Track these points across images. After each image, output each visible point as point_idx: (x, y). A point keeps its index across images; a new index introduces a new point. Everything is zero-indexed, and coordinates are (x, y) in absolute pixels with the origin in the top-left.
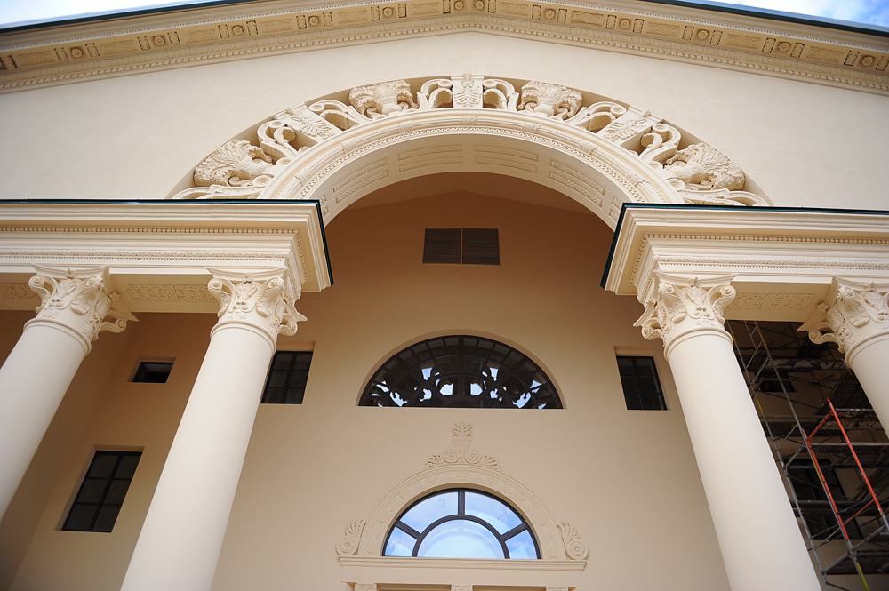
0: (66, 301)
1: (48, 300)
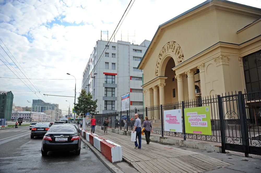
0: (189, 74)
1: (177, 78)
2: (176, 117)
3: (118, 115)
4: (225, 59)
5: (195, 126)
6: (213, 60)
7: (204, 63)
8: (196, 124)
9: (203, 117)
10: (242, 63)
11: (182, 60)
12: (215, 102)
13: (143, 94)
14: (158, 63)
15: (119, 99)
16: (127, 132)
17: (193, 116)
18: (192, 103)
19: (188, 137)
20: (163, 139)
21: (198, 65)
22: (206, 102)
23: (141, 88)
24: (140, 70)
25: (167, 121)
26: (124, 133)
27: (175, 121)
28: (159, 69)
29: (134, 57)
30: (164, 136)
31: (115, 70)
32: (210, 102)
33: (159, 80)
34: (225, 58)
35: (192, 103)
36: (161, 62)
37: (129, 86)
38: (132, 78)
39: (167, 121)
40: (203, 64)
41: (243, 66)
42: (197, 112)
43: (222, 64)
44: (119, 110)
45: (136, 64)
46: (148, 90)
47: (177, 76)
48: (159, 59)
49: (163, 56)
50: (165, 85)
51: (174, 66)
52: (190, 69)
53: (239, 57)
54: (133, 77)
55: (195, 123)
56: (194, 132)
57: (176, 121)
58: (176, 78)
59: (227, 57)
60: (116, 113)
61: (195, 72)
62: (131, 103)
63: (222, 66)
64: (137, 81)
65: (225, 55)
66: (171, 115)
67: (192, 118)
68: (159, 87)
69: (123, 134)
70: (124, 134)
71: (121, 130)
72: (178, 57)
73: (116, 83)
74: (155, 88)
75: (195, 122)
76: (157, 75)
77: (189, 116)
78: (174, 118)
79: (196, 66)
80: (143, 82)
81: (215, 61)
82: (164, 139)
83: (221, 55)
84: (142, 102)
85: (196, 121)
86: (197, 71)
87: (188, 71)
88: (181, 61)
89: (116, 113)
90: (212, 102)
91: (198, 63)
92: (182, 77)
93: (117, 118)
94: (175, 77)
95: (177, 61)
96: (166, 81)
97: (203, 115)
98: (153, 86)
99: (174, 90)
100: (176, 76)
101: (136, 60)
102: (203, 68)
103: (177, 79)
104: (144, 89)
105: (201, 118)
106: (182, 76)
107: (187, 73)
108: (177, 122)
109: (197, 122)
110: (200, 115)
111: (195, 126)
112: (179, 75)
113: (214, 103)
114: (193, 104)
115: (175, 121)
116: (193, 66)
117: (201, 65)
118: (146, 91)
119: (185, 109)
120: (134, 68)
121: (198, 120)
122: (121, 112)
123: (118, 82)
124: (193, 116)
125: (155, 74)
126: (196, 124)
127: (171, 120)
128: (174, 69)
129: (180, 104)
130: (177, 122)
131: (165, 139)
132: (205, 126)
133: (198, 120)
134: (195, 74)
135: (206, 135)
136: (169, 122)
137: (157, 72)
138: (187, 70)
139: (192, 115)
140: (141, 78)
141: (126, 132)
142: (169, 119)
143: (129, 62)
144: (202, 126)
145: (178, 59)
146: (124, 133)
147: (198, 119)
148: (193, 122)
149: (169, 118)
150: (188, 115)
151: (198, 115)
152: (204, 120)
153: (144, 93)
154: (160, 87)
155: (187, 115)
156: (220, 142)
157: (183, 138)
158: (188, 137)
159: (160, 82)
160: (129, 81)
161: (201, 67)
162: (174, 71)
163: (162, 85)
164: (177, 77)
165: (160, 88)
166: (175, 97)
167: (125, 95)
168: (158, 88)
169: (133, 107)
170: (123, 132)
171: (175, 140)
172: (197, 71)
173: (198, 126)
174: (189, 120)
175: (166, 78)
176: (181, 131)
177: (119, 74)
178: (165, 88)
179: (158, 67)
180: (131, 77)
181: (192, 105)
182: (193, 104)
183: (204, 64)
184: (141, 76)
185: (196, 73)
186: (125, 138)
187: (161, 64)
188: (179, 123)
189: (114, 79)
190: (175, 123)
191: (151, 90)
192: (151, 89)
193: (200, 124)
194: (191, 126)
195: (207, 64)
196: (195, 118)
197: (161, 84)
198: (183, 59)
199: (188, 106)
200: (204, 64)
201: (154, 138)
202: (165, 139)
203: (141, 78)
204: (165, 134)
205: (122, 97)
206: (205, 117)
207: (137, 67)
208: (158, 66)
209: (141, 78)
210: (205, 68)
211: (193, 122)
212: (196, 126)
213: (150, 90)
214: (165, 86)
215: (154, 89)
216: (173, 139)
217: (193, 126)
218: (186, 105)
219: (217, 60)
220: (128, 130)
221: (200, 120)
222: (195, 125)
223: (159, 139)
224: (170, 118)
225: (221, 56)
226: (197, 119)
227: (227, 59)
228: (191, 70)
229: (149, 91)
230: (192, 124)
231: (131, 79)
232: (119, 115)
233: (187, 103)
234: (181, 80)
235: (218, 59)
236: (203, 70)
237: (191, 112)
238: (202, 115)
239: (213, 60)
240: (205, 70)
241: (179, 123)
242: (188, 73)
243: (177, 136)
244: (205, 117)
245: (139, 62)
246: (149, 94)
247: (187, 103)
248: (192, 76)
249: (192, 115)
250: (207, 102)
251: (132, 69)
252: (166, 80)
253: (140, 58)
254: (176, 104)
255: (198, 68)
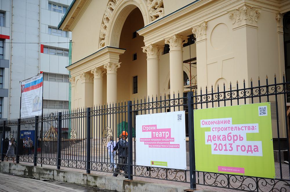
0: (173, 44)
1: (147, 53)
2: (169, 130)
3: (9, 129)
4: (252, 14)
5: (223, 153)
6: (228, 16)
7: (206, 21)
8: (228, 147)
9: (251, 131)
10: (282, 26)
11: (159, 13)
12: (228, 99)
13: (70, 83)
14: (107, 18)
15: (15, 92)
16: (35, 170)
17: (219, 129)
18: (174, 102)
19: (201, 182)
20: (131, 186)
21: (194, 26)
22: (219, 98)
23: (66, 72)
24: (64, 33)
25: (145, 141)
26: (25, 171)
27: (168, 140)
28: (108, 33)
29: (50, 3)
30: (134, 178)
31: (4, 28)
32: (204, 100)
33: (108, 56)
34: (252, 13)
35: (174, 102)
36: (113, 16)
37: (38, 67)
38: (45, 49)
39: (145, 141)
40: (204, 24)
41: (283, 32)
42: (230, 119)
43: (245, 24)
44: (14, 117)
45: (56, 18)
46: (81, 77)
47: (148, 47)
48: (109, 10)
49: (117, 3)
50: (119, 66)
51: (141, 25)
52: (176, 33)
53: (277, 14)
54: (47, 47)
55: (225, 145)
56: (220, 168)
57: (169, 141)
58: (144, 51)
59: (256, 10)
60: (5, 124)
61: (184, 41)
62: (46, 103)
63: (244, 29)
64: (57, 57)
65: (252, 6)
66: (156, 126)
67: (216, 133)
68: (106, 70)
69: (23, 173)
70: (25, 174)
71: (19, 166)
72: (150, 6)
73: (7, 57)
74: (97, 72)
75: (223, 143)
76: (103, 45)
77: (208, 129)
78: (164, 132)
79: (190, 28)
80: (70, 58)
81: (231, 17)
82: (134, 186)
83: (246, 5)
84: (68, 101)
85: (227, 142)
86: (188, 39)
87: (170, 38)
88: (157, 17)
89: (5, 124)
90: (221, 98)
91: (214, 8)
92: (156, 51)
93: (8, 135)
94: (143, 49)
95: (148, 16)
96: (122, 58)
97: (251, 125)
98: (92, 67)
99: (135, 79)
100: (144, 48)
101: (55, 10)
102: (203, 32)
103: (146, 54)
104: (73, 74)
105: (243, 133)
106: (158, 48)
107: (169, 42)
108: (171, 143)
109: (231, 144)
110: (240, 126)
111: (223, 153)
112: (151, 46)
113: (238, 99)
114: (176, 104)
115: (168, 140)
116: (182, 27)
117: (199, 26)
118: (76, 79)
119: (197, 113)
120: (50, 27)
121: (235, 138)
122: (19, 120)
123: (12, 56)
124: (219, 129)
125: (99, 43)
126: (228, 147)
127: (156, 138)
128: (140, 33)
129: (179, 99)
130: (171, 143)
131: (139, 185)
132: (255, 154)
133: (235, 138)
134: (185, 45)
135: (257, 178)
136: (150, 143)
137: (104, 39)
138: (170, 36)
139: (215, 126)
140: (66, 52)
141: (30, 168)
142: (151, 137)
143: (39, 13)
144: (245, 154)
145: (151, 12)
146: (25, 171)
147: (234, 136)
148: (218, 142)
149: (151, 132)
150: (205, 126)
151: (234, 126)
152: (250, 137)
153: (72, 82)
154: (108, 69)
155: (202, 126)
156: (198, 172)
157: (189, 185)
158: (201, 182)
159: (109, 60)
160: (39, 56)
161: (200, 29)
162: (142, 38)
163: (114, 67)
164: (146, 51)
165: (108, 72)
166: (137, 93)
167: (32, 81)
168: (103, 72)
169: (47, 112)
170: (24, 168)
171: (165, 188)
172: (188, 39)
173: (234, 153)
174: (206, 138)
175: (122, 52)
176: (183, 165)
177: (15, 37)
178: (120, 73)
179: (106, 27)
180: (43, 48)
181: (207, 102)
182: (176, 104)
183: (206, 23)
184: (66, 46)
185: (186, 42)
186: (31, 185)
187: (113, 22)
188: (177, 146)
189: (3, 47)
190: (168, 146)
191: (89, 77)
192: (90, 75)
193: (239, 148)
194: (214, 152)
195: (212, 25)
196: (226, 133)
197: (111, 64)
198: (161, 11)
199: (143, 111)
200: (206, 23)
201: (107, 183)
202: (139, 185)
203: (67, 50)
204: (138, 173)
205: (23, 83)
206: (257, 131)
207: (56, 25)
208: (106, 24)
209: (66, 52)
210: (209, 32)
211: (218, 142)
212: (228, 153)
213: (85, 76)
214: (118, 69)
215: (95, 74)
216: (161, 187)
217: (218, 153)
218: (199, 101)
219: (235, 17)
220: (35, 165)
221: (241, 139)
222: (226, 150)
223: (122, 185)
224: (152, 134)
225: (245, 8)
226: (232, 135)
227: (255, 15)
228: (179, 36)
229: (84, 78)
230: (215, 150)
231: (42, 51)
232: (14, 128)
233: (201, 96)
234: (155, 56)
235: (238, 12)
236: (204, 37)
237: (213, 118)
238: (247, 125)
239: (228, 16)
240: (208, 37)
241: (177, 146)
242: (170, 41)
243: (172, 178)
244: (257, 131)
245: (63, 15)
246: (84, 84)
247: (201, 96)
248: (179, 48)
249: (215, 126)
250: (221, 98)
251: (44, 29)
252: (121, 56)
253: (65, 7)
254: (140, 103)
255: (193, 33)
